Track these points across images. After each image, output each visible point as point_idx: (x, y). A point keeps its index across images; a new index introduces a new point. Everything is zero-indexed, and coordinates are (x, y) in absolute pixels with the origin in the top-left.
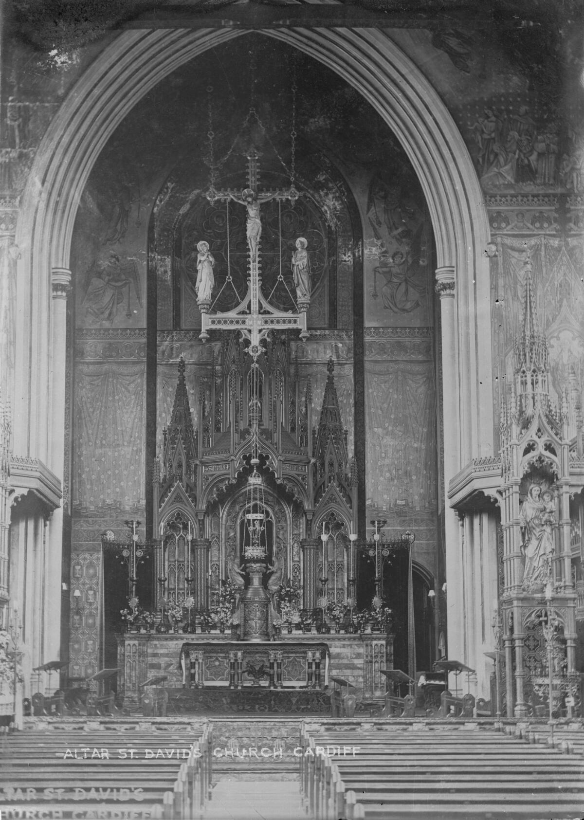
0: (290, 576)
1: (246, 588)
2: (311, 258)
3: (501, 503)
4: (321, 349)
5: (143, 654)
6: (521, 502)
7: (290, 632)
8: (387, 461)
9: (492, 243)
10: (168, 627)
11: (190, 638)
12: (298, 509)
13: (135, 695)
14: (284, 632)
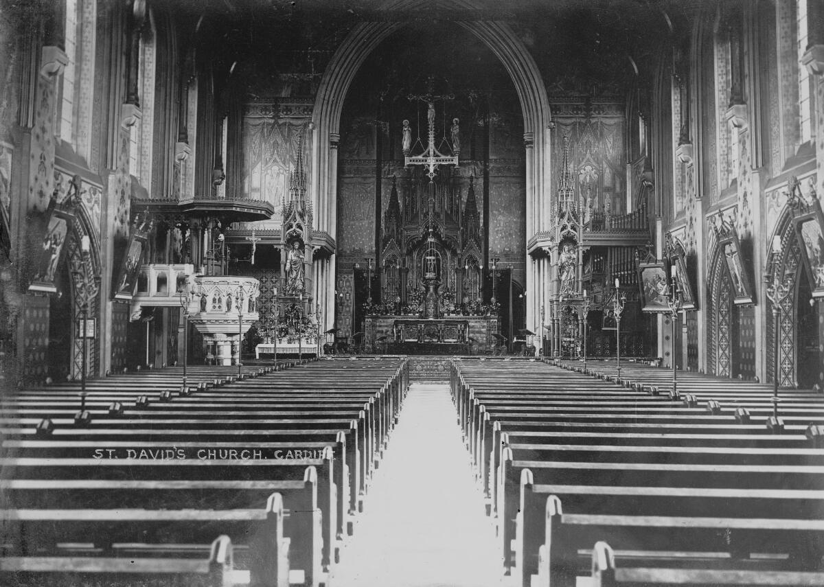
0: (449, 286)
1: (427, 293)
2: (460, 128)
3: (551, 254)
4: (467, 169)
5: (374, 326)
6: (559, 254)
7: (449, 315)
8: (500, 228)
9: (552, 122)
10: (387, 312)
11: (399, 318)
12: (454, 253)
13: (371, 346)
14: (446, 315)
